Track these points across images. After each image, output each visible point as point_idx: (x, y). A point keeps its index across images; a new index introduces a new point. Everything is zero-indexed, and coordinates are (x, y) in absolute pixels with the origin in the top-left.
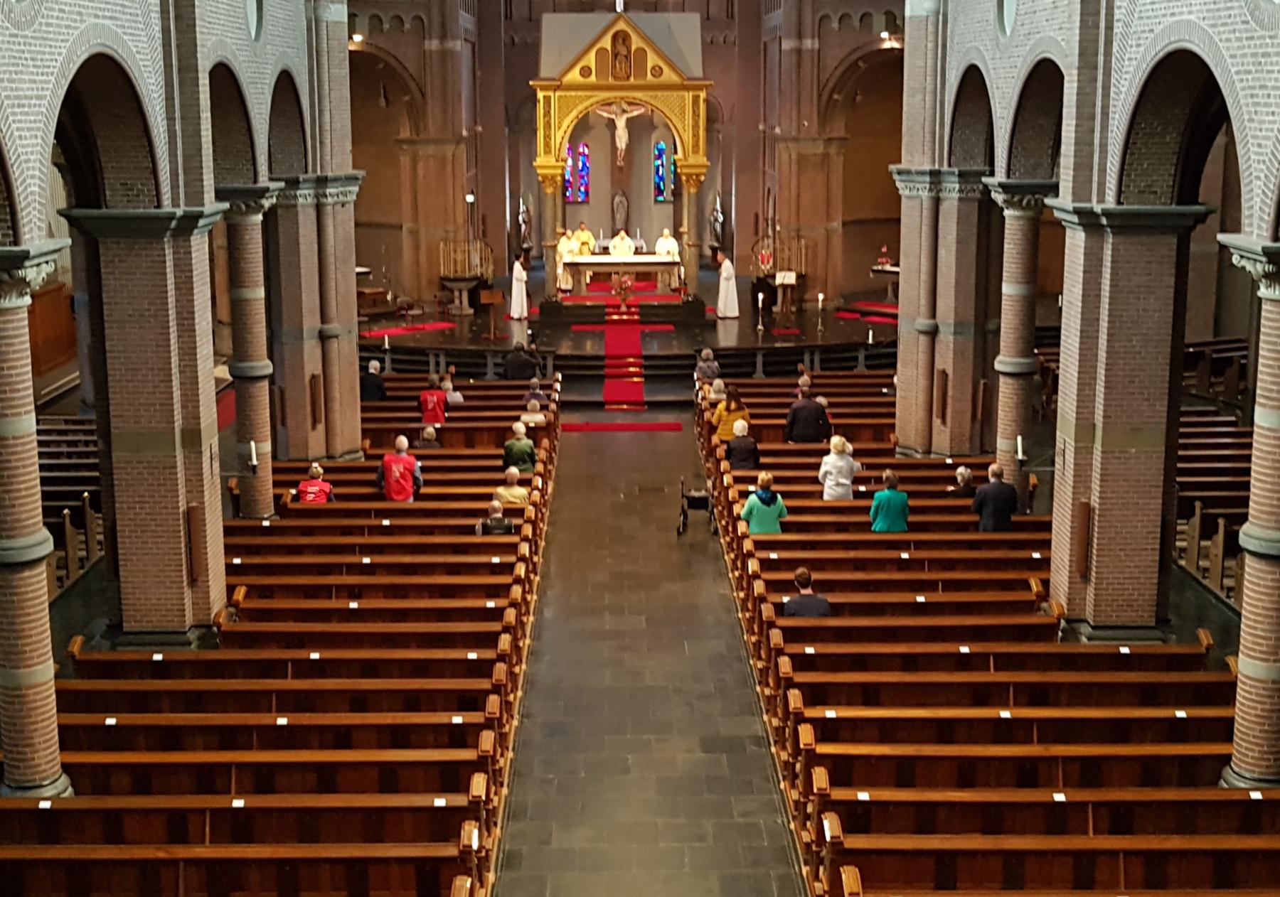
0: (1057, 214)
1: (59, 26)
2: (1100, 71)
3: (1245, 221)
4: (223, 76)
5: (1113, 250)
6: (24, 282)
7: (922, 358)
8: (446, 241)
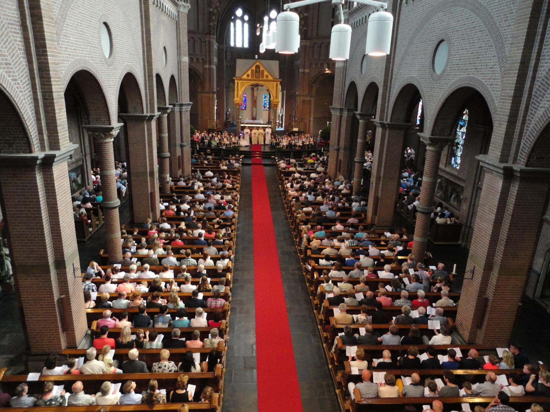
0: (375, 123)
1: (119, 65)
2: (389, 87)
3: (425, 130)
4: (158, 76)
5: (389, 133)
6: (112, 135)
7: (335, 156)
8: (210, 119)
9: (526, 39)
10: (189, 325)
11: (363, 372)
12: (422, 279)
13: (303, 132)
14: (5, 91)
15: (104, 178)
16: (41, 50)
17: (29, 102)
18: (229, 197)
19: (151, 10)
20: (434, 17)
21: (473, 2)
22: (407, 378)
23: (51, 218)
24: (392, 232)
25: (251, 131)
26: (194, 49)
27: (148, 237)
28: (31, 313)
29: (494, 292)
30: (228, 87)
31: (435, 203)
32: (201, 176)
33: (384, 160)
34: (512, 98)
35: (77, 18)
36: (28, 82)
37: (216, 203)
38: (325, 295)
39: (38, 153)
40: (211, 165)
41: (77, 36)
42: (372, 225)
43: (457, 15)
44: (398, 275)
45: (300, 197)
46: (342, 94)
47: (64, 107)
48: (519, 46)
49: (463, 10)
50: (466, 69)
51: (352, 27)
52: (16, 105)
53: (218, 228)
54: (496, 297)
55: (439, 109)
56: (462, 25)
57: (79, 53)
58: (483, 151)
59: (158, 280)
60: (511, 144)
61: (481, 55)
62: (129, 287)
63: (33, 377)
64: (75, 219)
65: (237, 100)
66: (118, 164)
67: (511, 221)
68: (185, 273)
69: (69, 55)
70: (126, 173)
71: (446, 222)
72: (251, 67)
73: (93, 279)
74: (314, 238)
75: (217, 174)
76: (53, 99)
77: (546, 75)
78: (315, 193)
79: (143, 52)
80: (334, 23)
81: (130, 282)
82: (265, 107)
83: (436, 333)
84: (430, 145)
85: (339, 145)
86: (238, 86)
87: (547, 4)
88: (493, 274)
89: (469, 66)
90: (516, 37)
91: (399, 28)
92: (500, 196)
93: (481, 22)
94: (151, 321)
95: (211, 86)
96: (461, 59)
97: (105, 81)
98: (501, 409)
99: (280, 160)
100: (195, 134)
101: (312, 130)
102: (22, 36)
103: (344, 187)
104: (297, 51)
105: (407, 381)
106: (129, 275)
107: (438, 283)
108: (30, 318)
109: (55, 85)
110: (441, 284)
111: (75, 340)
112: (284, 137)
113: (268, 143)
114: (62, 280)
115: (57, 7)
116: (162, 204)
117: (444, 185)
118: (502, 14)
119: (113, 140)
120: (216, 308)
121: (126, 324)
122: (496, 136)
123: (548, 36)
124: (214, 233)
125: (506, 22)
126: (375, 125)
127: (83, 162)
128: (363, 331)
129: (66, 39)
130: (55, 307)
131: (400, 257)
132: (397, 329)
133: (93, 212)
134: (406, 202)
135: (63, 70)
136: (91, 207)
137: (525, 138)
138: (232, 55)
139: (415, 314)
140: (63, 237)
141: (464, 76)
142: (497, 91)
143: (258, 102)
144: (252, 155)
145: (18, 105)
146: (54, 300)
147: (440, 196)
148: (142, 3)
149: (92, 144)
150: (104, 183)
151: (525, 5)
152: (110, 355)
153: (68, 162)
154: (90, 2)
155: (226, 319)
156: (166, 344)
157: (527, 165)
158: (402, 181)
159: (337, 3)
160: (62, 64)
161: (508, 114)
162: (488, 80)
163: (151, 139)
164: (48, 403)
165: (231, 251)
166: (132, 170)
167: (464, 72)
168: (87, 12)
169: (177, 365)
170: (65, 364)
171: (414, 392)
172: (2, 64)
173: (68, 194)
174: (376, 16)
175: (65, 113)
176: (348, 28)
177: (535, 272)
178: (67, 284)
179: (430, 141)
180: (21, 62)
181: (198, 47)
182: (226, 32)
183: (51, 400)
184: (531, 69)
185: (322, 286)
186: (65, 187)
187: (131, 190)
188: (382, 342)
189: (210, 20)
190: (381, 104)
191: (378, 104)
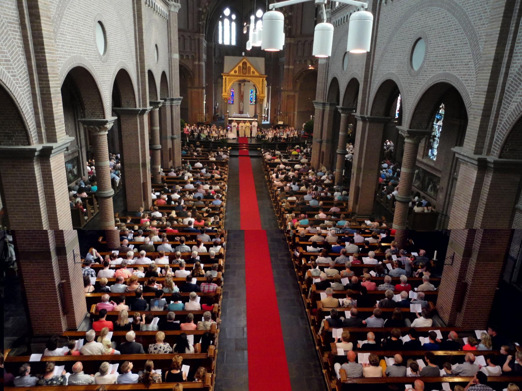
0: (355, 117)
1: (113, 62)
2: (369, 83)
3: (403, 123)
4: (150, 73)
5: (369, 127)
6: (106, 128)
7: (318, 148)
8: (199, 113)
9: (499, 37)
10: (183, 308)
11: (348, 353)
12: (404, 265)
13: (287, 125)
14: (5, 87)
15: (99, 169)
16: (39, 47)
17: (27, 97)
18: (218, 187)
19: (143, 9)
20: (412, 16)
21: (449, 2)
22: (390, 359)
23: (48, 207)
24: (372, 221)
25: (238, 124)
26: (185, 46)
27: (140, 225)
28: (33, 297)
29: (473, 277)
30: (216, 83)
31: (412, 192)
32: (191, 167)
33: (364, 152)
34: (486, 93)
35: (73, 17)
36: (26, 78)
37: (205, 192)
38: (312, 280)
39: (37, 146)
40: (200, 156)
41: (73, 34)
42: (353, 213)
43: (434, 14)
44: (382, 261)
45: (285, 187)
46: (324, 89)
47: (61, 101)
48: (493, 44)
49: (440, 9)
50: (442, 66)
51: (334, 25)
52: (15, 100)
53: (207, 217)
54: (475, 282)
55: (417, 103)
56: (438, 24)
57: (75, 50)
58: (458, 143)
59: (153, 265)
60: (485, 137)
61: (457, 52)
62: (126, 273)
63: (35, 357)
64: (71, 207)
65: (225, 94)
66: (112, 156)
67: (485, 210)
68: (180, 259)
69: (65, 52)
70: (120, 164)
71: (424, 211)
72: (238, 64)
73: (92, 265)
74: (298, 225)
75: (206, 166)
76: (50, 94)
77: (519, 72)
78: (299, 183)
79: (136, 49)
80: (317, 22)
81: (127, 268)
82: (251, 102)
83: (418, 316)
84: (408, 137)
85: (321, 137)
86: (225, 82)
87: (519, 4)
88: (472, 260)
89: (446, 63)
90: (490, 35)
91: (379, 27)
92: (475, 186)
93: (457, 21)
94: (148, 305)
95: (200, 82)
96: (438, 56)
97: (100, 77)
98: (479, 388)
99: (266, 152)
100: (185, 127)
101: (296, 123)
102: (21, 34)
103: (327, 178)
104: (282, 49)
105: (391, 362)
106: (126, 261)
107: (419, 268)
108: (32, 302)
109: (52, 81)
110: (423, 269)
111: (75, 323)
112: (270, 130)
113: (255, 136)
114: (63, 266)
115: (54, 6)
116: (154, 194)
117: (421, 175)
118: (476, 14)
119: (107, 133)
120: (209, 292)
121: (123, 308)
122: (471, 129)
123: (520, 34)
124: (203, 221)
125: (480, 21)
126: (356, 119)
127: (79, 153)
128: (348, 315)
129: (62, 37)
130: (56, 292)
131: (383, 244)
132: (380, 312)
133: (88, 202)
134: (385, 191)
135: (59, 66)
136: (87, 196)
137: (499, 131)
138: (220, 52)
139: (398, 298)
140: (60, 225)
141: (440, 72)
142: (472, 86)
143: (245, 97)
144: (239, 147)
145: (18, 99)
146: (55, 284)
147: (418, 186)
148: (135, 3)
149: (88, 136)
150: (99, 174)
151: (499, 4)
152: (108, 337)
153: (64, 154)
154: (85, 2)
155: (218, 303)
156: (161, 326)
157: (500, 157)
158: (381, 172)
159: (320, 3)
160: (59, 60)
161: (482, 108)
162: (463, 76)
163: (144, 132)
164: (49, 383)
165: (223, 238)
166: (125, 161)
167: (441, 68)
168: (83, 12)
169: (172, 346)
170: (66, 346)
171: (397, 372)
172: (2, 60)
173: (65, 184)
174: (357, 15)
175: (62, 107)
176: (331, 26)
177: (512, 258)
178: (68, 269)
179: (408, 134)
180: (20, 59)
181: (188, 45)
182: (214, 30)
183: (52, 380)
184: (504, 65)
185: (310, 271)
186: (62, 177)
187: (125, 181)
188: (366, 324)
189: (199, 19)
190: (362, 99)
191: (359, 99)
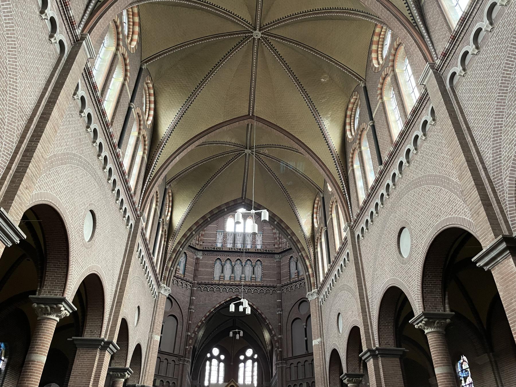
2: (368, 313)
